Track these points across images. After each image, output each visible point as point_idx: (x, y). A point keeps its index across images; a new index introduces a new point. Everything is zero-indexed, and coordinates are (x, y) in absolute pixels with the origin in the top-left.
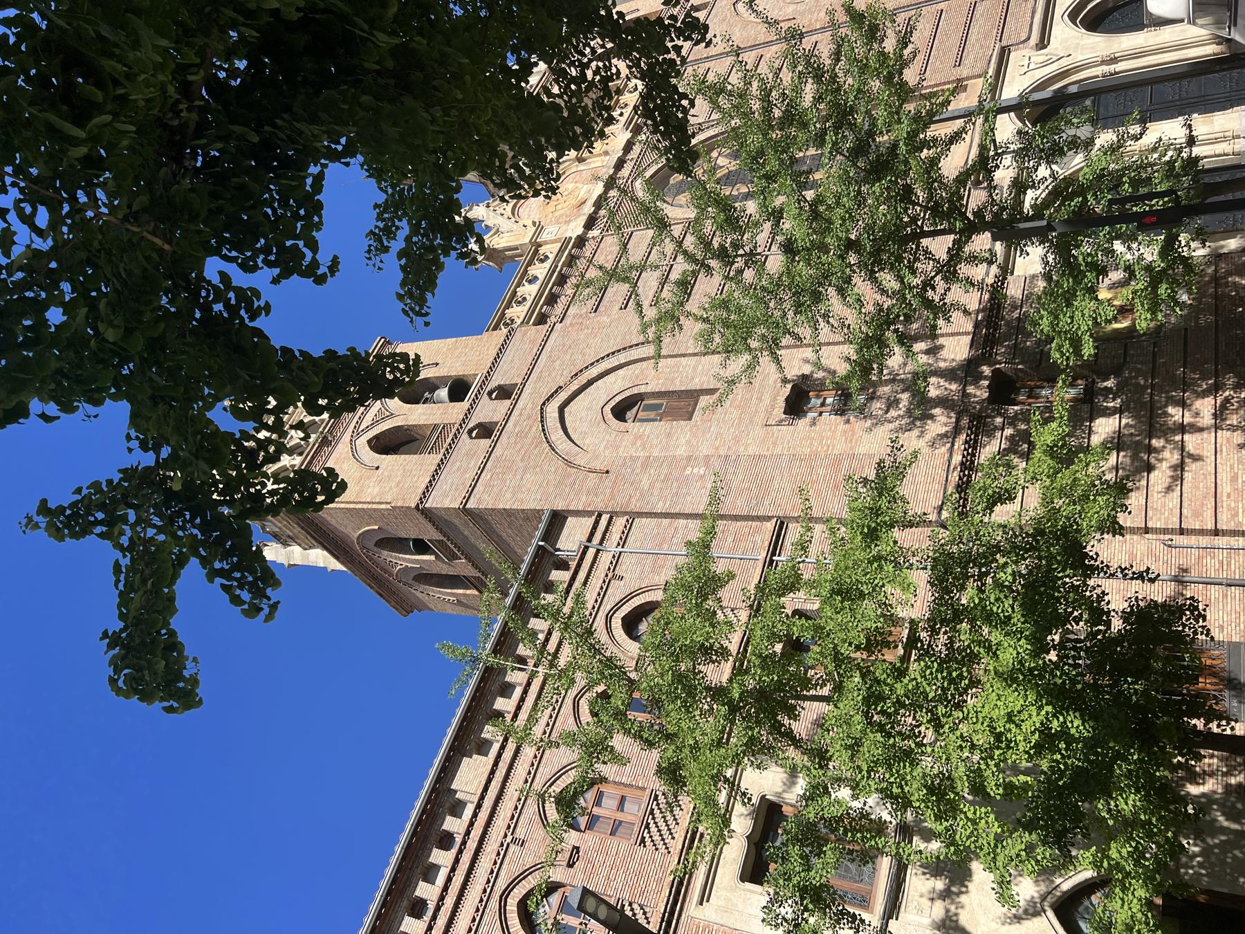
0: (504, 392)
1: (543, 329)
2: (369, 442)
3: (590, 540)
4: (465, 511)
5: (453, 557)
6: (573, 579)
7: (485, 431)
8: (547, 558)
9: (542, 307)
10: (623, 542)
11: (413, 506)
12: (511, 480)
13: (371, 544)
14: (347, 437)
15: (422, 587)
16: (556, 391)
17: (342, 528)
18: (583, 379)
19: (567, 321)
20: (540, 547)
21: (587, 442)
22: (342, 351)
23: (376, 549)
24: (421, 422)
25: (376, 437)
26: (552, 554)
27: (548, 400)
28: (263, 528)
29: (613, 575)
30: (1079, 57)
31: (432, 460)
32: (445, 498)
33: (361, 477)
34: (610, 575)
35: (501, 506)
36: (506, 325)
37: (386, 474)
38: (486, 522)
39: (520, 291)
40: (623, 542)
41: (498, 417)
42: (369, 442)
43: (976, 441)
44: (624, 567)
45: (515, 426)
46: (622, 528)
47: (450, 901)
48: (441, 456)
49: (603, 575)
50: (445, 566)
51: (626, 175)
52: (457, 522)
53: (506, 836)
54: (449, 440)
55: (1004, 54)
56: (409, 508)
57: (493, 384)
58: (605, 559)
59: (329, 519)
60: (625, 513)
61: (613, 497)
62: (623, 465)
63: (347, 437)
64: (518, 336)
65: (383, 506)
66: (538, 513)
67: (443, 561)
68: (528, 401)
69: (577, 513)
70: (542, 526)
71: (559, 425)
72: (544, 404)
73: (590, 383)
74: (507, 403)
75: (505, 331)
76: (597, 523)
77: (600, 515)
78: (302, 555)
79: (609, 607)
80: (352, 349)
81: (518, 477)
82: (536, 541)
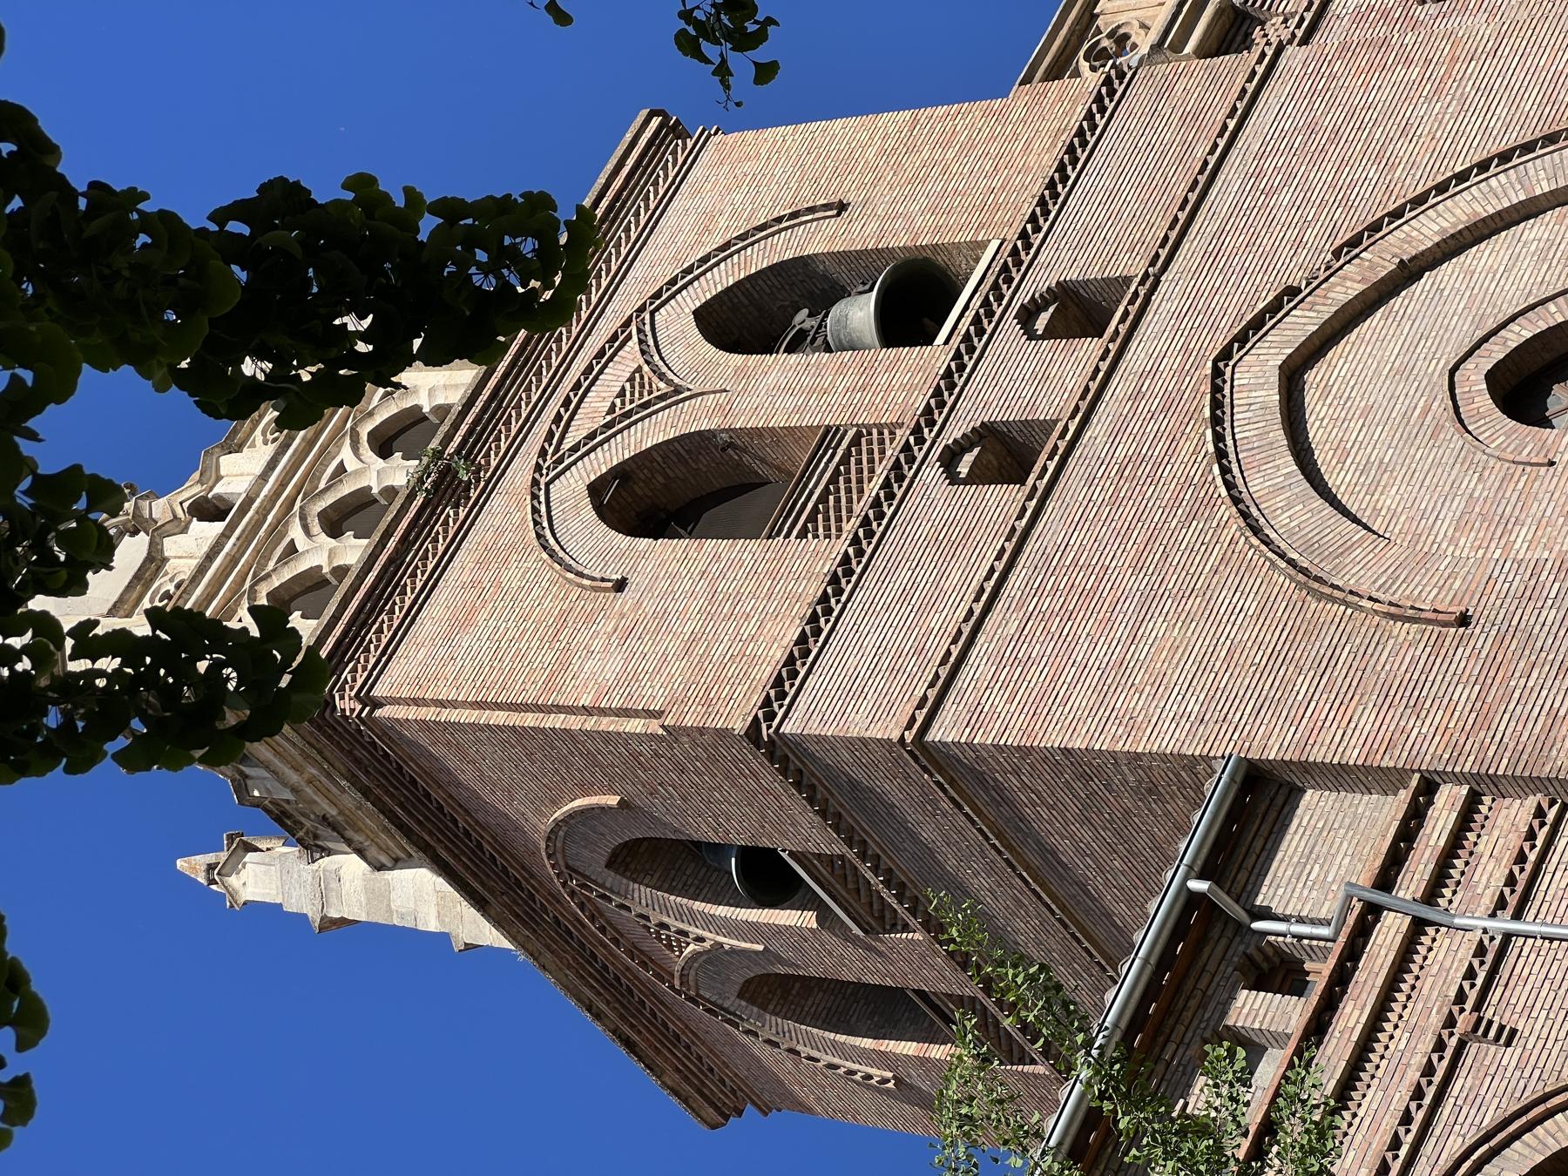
0: (1079, 311)
1: (1236, 67)
2: (595, 490)
3: (1386, 879)
4: (922, 751)
5: (879, 921)
6: (1317, 1028)
7: (1006, 454)
8: (1217, 946)
10: (1519, 895)
11: (739, 725)
12: (1104, 646)
13: (594, 861)
14: (520, 473)
15: (773, 1025)
16: (1275, 307)
17: (495, 799)
18: (1379, 260)
19: (1331, 35)
20: (1193, 900)
21: (1388, 501)
22: (326, 189)
23: (611, 878)
24: (779, 421)
25: (622, 473)
26: (1241, 929)
27: (1242, 338)
28: (242, 788)
29: (1473, 1024)
31: (808, 560)
32: (852, 705)
33: (564, 617)
34: (1464, 1022)
35: (1054, 739)
36: (1098, 56)
37: (649, 606)
38: (1001, 798)
40: (1519, 895)
42: (595, 490)
44: (1519, 995)
45: (1114, 436)
46: (1515, 841)
48: (842, 545)
49: (1436, 1020)
50: (851, 952)
52: (892, 790)
54: (873, 488)
56: (724, 734)
58: (1445, 962)
59: (452, 762)
60: (1526, 784)
61: (1482, 715)
62: (1528, 595)
63: (520, 473)
64: (1139, 96)
65: (635, 726)
66: (1192, 768)
67: (855, 940)
68: (1168, 345)
69: (1341, 777)
70: (1203, 821)
71: (1279, 436)
72: (1226, 354)
73: (1409, 273)
74: (1089, 350)
75: (1090, 79)
76: (1415, 817)
77: (1428, 788)
78: (370, 891)
79: (1455, 1146)
80: (362, 183)
81: (1121, 631)
82: (1182, 877)
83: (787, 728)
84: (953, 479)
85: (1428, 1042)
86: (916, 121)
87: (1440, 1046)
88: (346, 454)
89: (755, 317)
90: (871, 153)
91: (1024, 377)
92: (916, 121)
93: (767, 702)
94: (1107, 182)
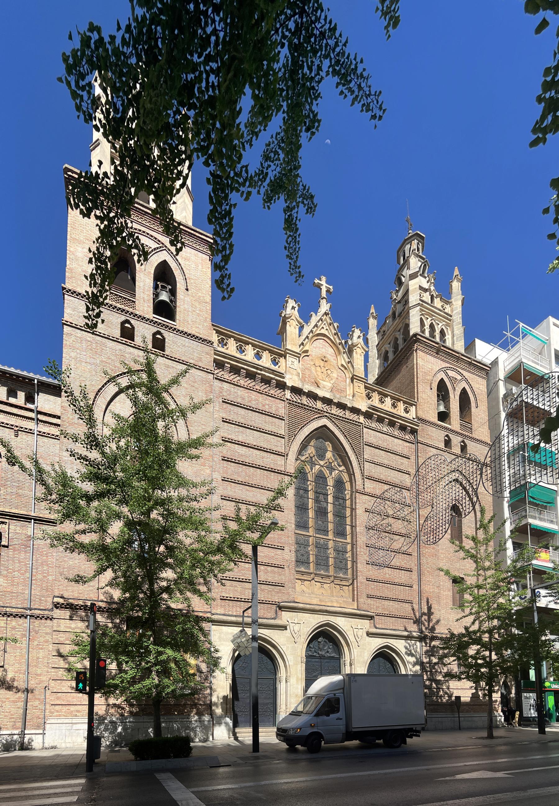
0: (464, 448)
1: (211, 366)
7: (448, 443)
9: (376, 414)
10: (41, 434)
19: (217, 383)
30: (355, 651)
39: (249, 348)
40: (41, 434)
41: (138, 340)
43: (103, 611)
44: (24, 437)
47: (15, 411)
49: (17, 424)
51: (333, 412)
53: (17, 427)
54: (118, 305)
55: (371, 618)
57: (166, 334)
58: (30, 425)
81: (88, 360)
83: (66, 296)
84: (123, 323)
85: (12, 423)
86: (206, 303)
87: (12, 425)
88: (430, 319)
89: (164, 276)
90: (200, 294)
91: (144, 332)
92: (206, 303)
93: (70, 290)
94: (187, 344)
